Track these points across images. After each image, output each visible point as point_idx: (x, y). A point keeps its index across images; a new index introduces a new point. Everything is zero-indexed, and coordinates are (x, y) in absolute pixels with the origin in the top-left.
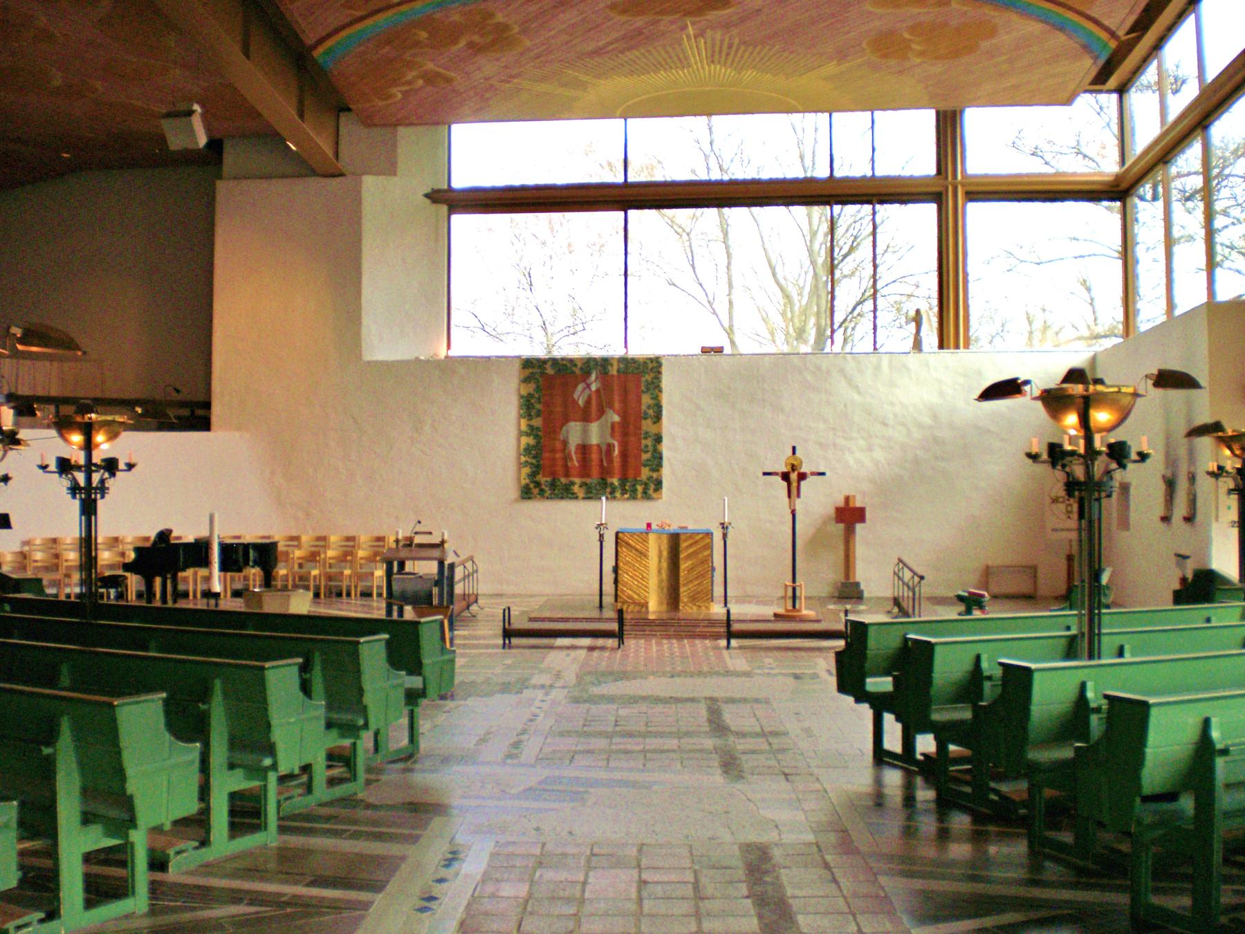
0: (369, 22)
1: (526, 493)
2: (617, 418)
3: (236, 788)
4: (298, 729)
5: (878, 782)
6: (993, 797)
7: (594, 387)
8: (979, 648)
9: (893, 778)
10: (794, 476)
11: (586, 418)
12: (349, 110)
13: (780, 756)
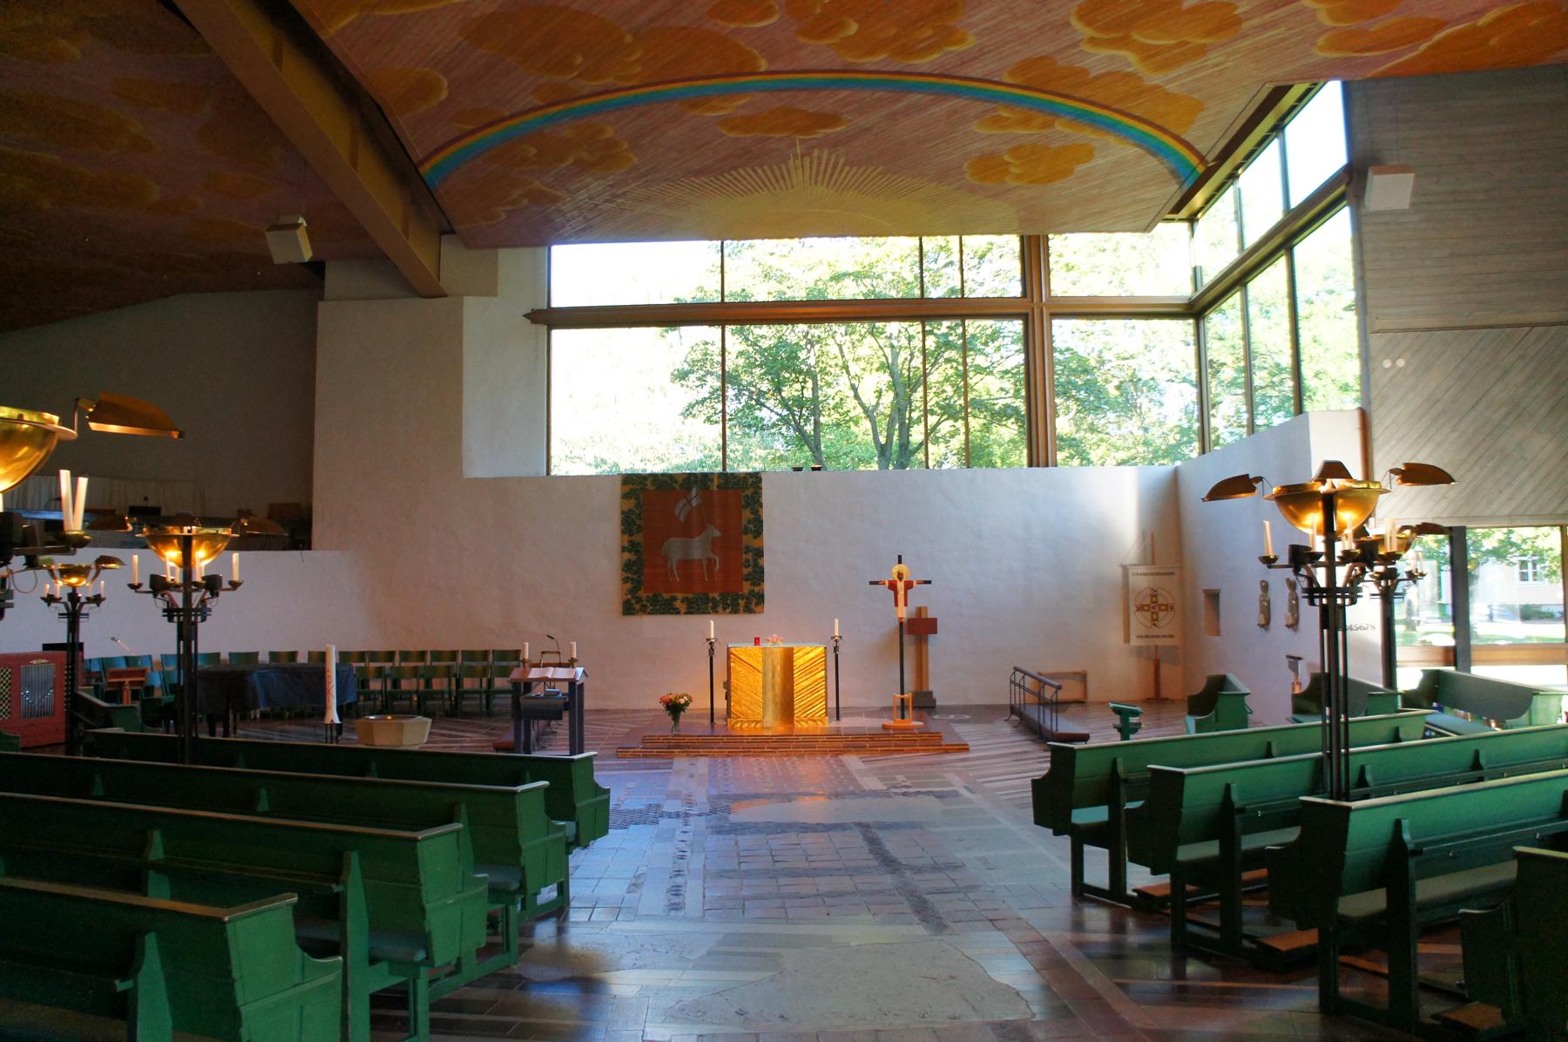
0: (479, 136)
1: (628, 609)
2: (717, 533)
3: (377, 987)
4: (452, 910)
5: (1078, 925)
6: (1246, 943)
7: (694, 503)
8: (1229, 778)
9: (1098, 918)
10: (901, 585)
11: (687, 531)
12: (453, 232)
13: (971, 896)
